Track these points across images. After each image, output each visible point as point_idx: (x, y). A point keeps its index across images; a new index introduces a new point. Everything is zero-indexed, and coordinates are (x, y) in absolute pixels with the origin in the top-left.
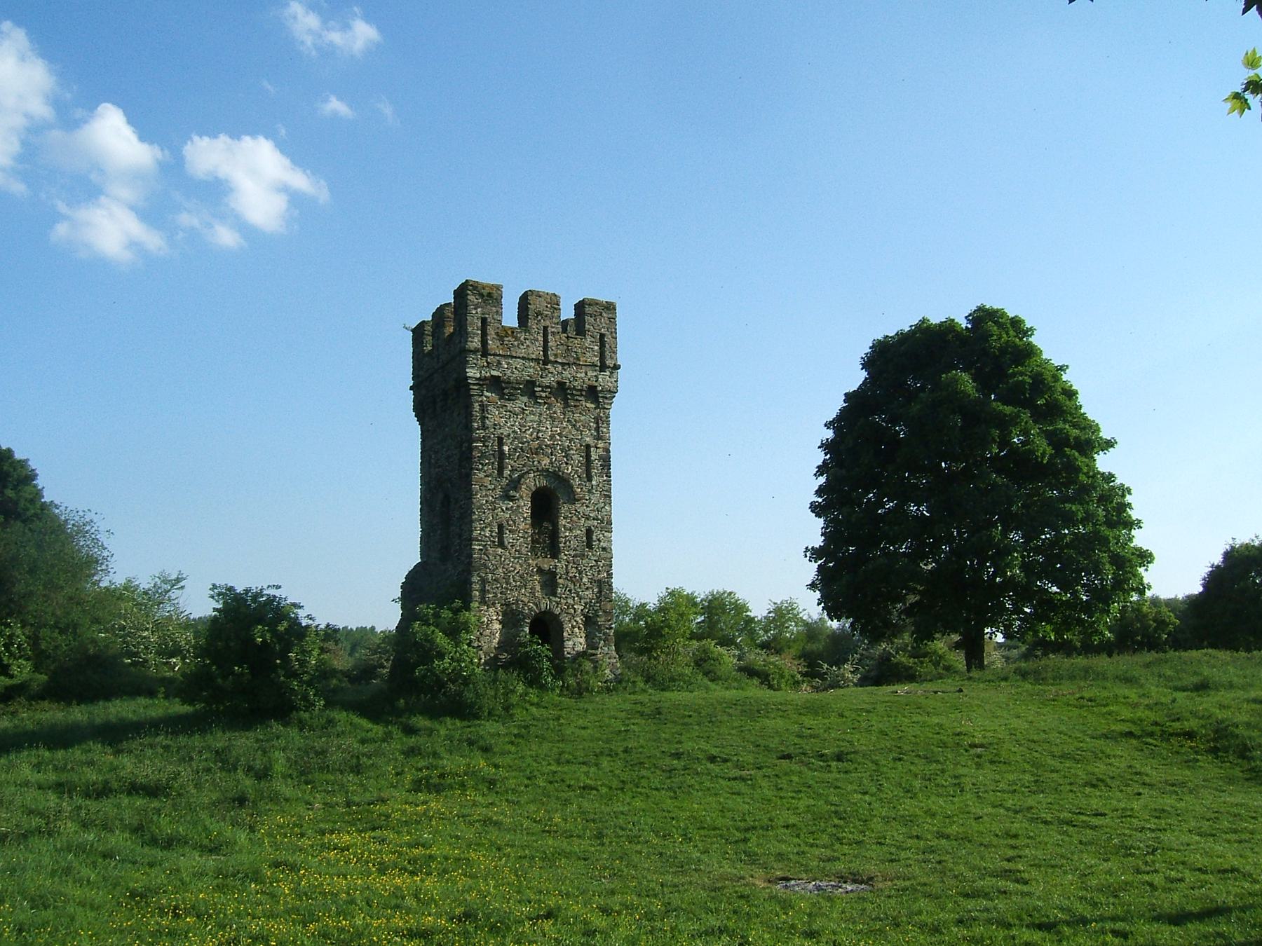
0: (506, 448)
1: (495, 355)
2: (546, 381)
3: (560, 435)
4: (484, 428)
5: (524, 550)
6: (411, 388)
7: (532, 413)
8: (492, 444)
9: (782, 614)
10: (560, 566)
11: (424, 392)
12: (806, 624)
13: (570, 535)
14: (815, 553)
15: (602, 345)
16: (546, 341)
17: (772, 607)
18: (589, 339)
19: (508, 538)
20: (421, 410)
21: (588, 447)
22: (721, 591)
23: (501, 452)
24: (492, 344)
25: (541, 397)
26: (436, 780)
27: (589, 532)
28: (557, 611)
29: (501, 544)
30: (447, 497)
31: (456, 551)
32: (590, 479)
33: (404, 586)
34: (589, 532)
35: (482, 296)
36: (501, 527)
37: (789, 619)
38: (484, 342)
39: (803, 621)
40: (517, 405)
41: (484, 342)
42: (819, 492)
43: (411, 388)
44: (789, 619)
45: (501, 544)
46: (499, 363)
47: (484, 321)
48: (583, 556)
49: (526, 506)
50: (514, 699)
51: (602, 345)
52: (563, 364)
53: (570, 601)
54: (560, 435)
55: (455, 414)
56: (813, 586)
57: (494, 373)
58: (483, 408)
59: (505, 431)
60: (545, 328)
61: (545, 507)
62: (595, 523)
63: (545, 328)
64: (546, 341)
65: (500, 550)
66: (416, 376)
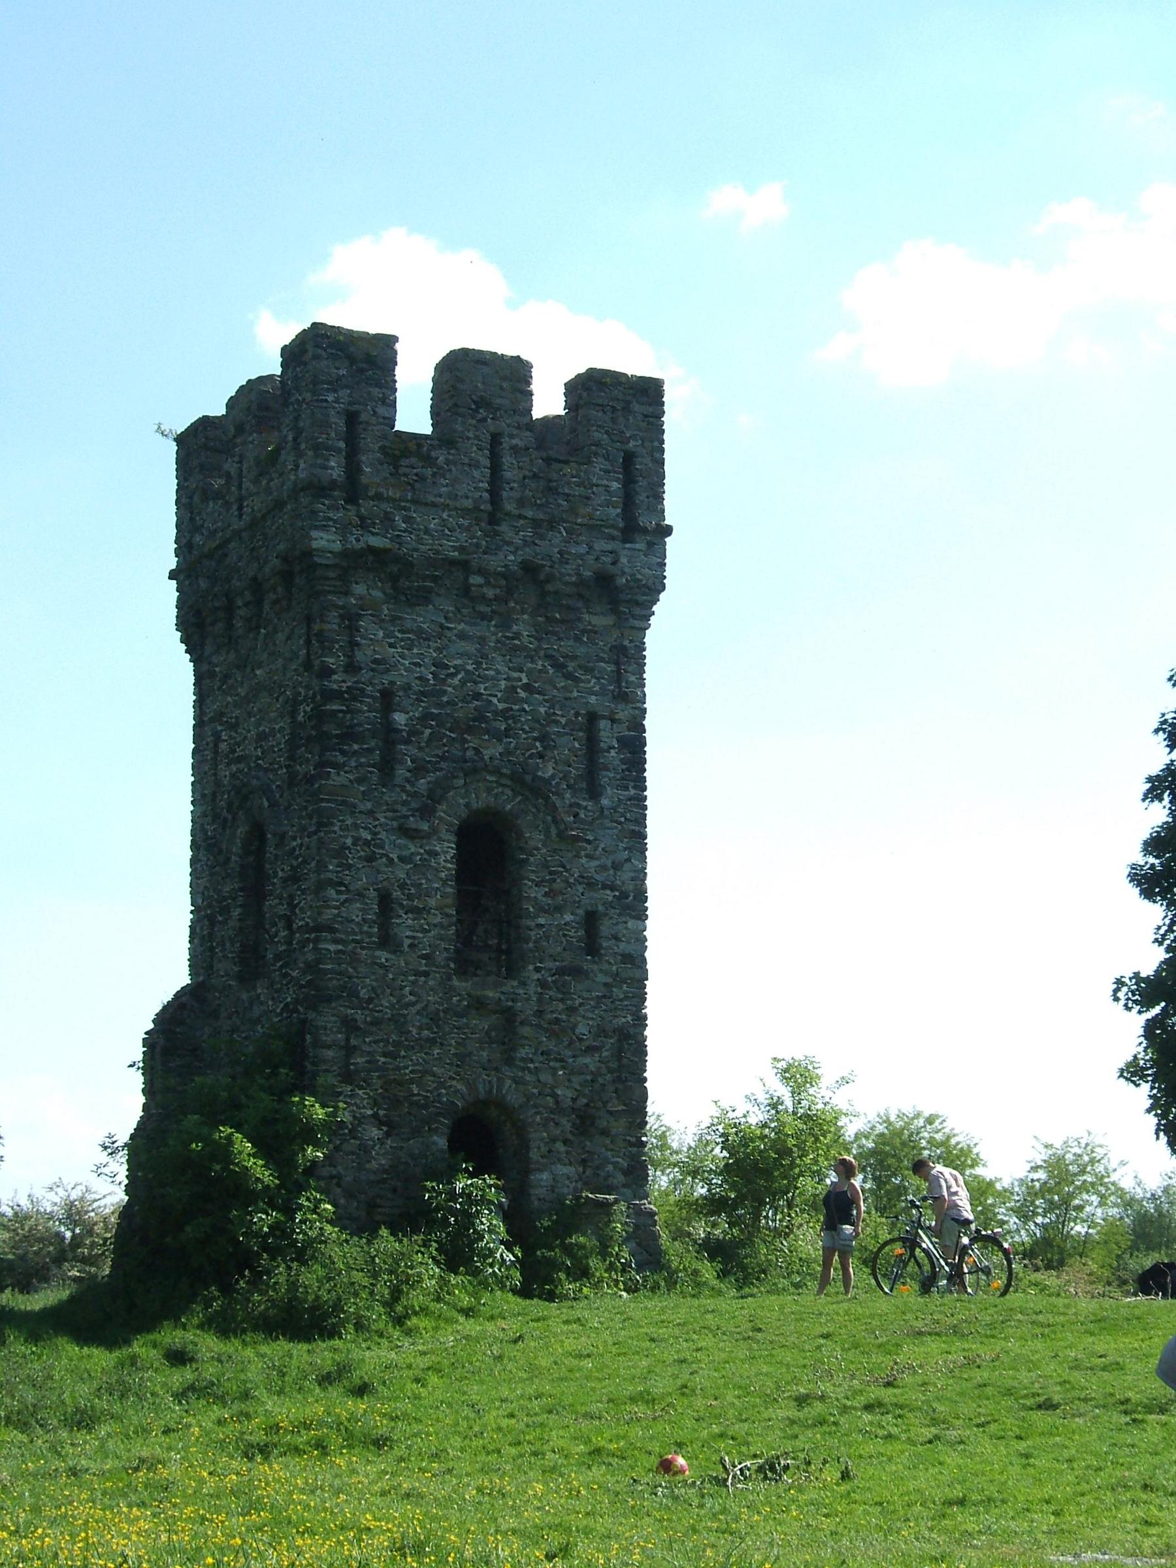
0: (400, 718)
1: (378, 497)
2: (495, 563)
3: (527, 688)
4: (352, 668)
5: (440, 957)
6: (173, 575)
7: (462, 636)
8: (366, 714)
9: (1063, 1180)
10: (525, 992)
11: (203, 584)
12: (1129, 1202)
13: (548, 925)
14: (1146, 991)
15: (629, 481)
16: (496, 468)
17: (1039, 1157)
18: (599, 464)
19: (404, 925)
20: (195, 625)
21: (593, 717)
22: (909, 1111)
23: (389, 729)
24: (370, 472)
25: (483, 598)
26: (260, 1437)
27: (591, 920)
28: (514, 1098)
29: (387, 940)
30: (258, 833)
31: (278, 957)
32: (594, 792)
33: (150, 1041)
34: (591, 920)
35: (352, 360)
36: (385, 900)
37: (1085, 1188)
38: (353, 469)
39: (1120, 1192)
40: (422, 618)
41: (353, 469)
42: (1153, 845)
43: (173, 575)
44: (1085, 1188)
45: (387, 940)
46: (388, 518)
47: (352, 419)
48: (577, 972)
49: (446, 850)
50: (415, 1298)
51: (629, 481)
52: (536, 523)
53: (546, 1077)
54: (527, 688)
55: (281, 637)
56: (1132, 1072)
57: (376, 542)
58: (350, 620)
59: (400, 676)
60: (495, 439)
61: (486, 853)
62: (609, 895)
63: (495, 439)
64: (496, 468)
65: (383, 956)
66: (184, 546)
